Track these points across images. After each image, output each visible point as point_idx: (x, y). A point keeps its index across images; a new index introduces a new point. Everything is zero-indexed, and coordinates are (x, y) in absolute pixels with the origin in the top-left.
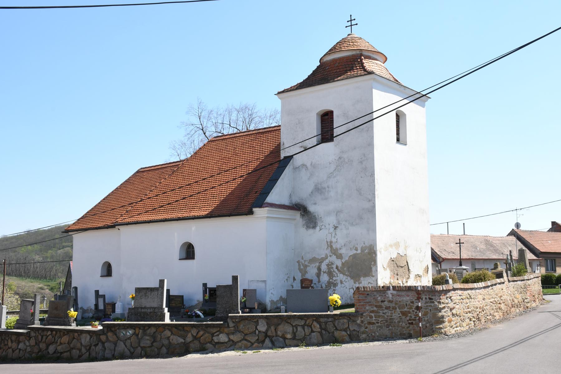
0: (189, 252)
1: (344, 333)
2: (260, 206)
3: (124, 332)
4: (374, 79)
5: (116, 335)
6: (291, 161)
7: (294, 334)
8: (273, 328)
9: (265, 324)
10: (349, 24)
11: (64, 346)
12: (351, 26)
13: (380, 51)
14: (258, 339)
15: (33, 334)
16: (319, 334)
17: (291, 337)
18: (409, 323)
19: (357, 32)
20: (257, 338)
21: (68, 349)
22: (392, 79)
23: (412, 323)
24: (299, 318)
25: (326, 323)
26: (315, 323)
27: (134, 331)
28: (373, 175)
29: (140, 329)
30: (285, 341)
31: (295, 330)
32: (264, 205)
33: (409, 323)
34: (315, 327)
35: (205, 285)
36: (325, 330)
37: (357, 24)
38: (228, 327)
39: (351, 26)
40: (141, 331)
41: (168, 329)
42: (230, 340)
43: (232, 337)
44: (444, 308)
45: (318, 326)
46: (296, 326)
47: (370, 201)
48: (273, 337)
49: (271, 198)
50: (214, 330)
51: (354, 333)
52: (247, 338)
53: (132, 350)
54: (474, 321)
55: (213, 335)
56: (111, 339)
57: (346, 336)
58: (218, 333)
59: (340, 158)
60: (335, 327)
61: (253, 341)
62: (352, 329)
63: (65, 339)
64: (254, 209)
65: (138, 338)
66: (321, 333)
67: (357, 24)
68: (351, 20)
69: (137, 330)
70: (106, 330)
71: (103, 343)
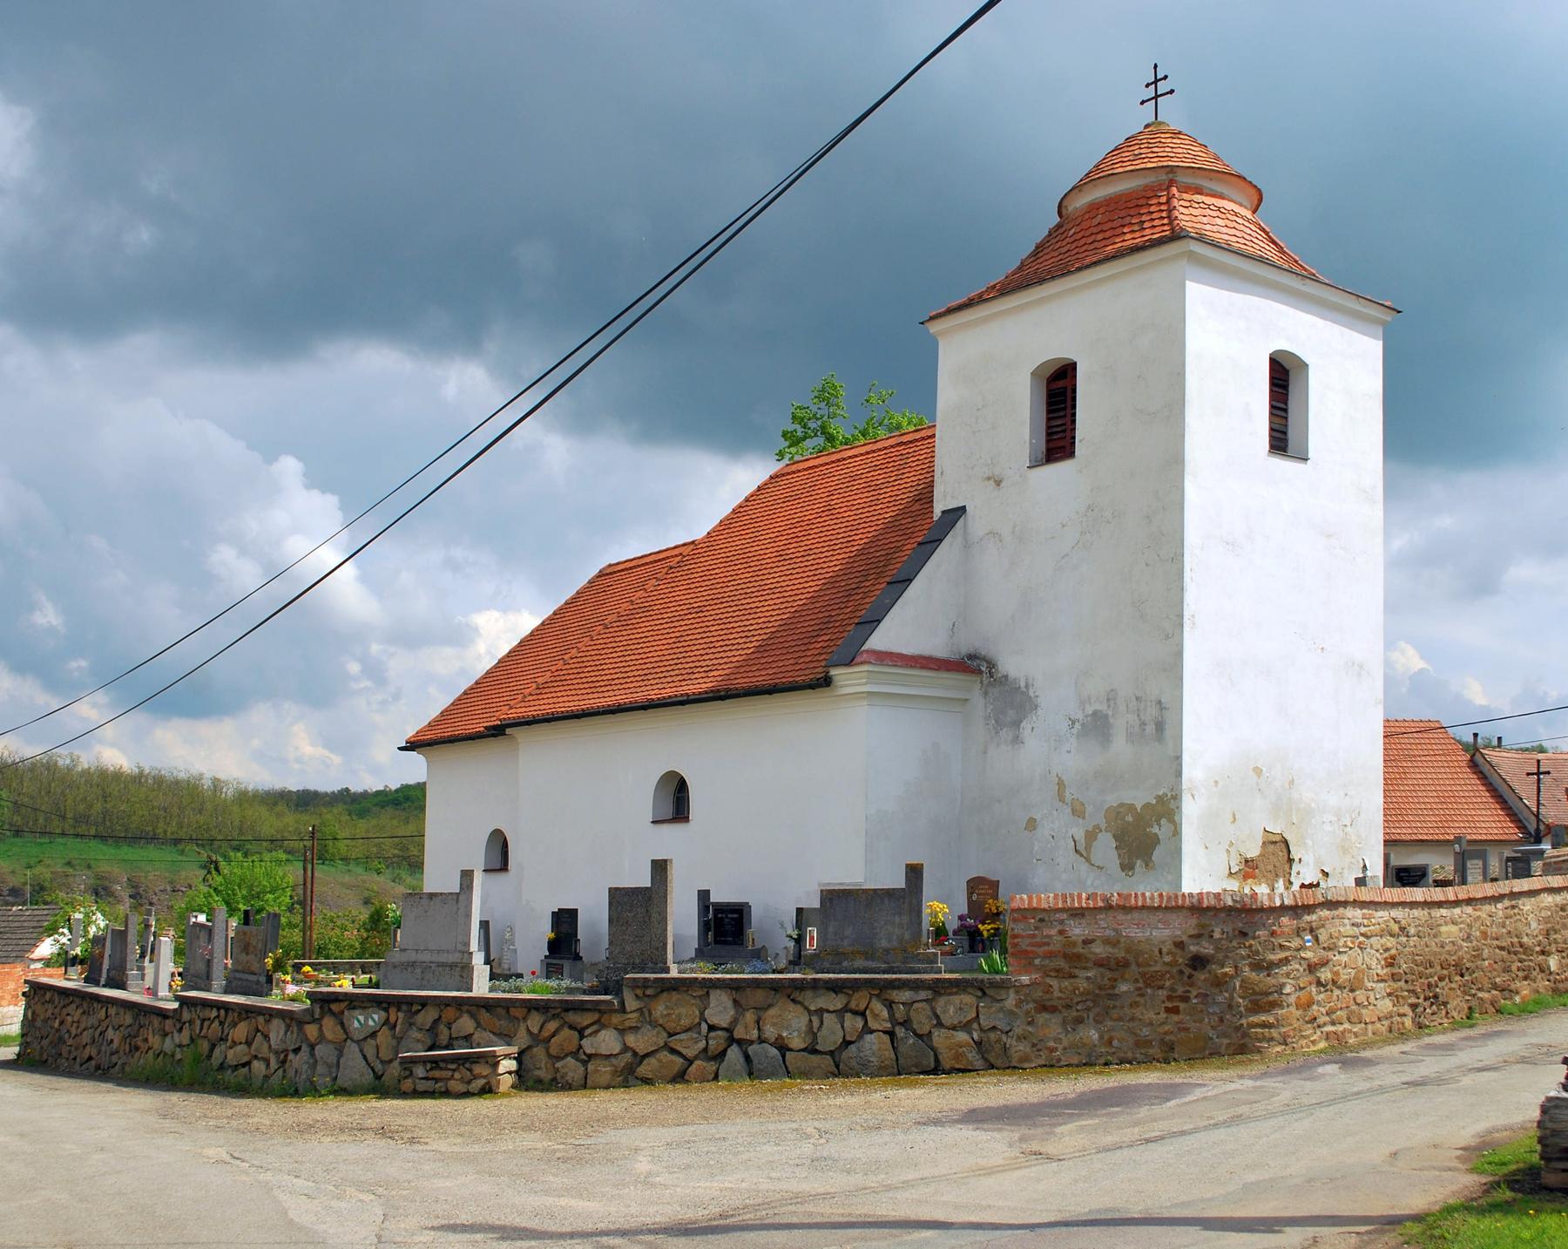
0: (676, 800)
1: (962, 1036)
2: (850, 663)
3: (361, 1018)
4: (1193, 257)
5: (342, 1024)
6: (960, 524)
7: (812, 1034)
8: (750, 1017)
9: (730, 1004)
10: (1151, 92)
11: (239, 1048)
12: (1156, 97)
13: (1237, 168)
14: (705, 1050)
15: (186, 1016)
16: (886, 1038)
17: (803, 1046)
18: (1168, 1010)
19: (1172, 113)
20: (702, 1044)
21: (246, 1059)
22: (1270, 252)
23: (1175, 1010)
24: (828, 989)
25: (908, 1005)
26: (877, 1006)
27: (383, 1014)
28: (1177, 558)
29: (399, 1010)
30: (784, 1057)
31: (816, 1023)
32: (858, 659)
33: (1168, 1010)
34: (876, 1016)
35: (704, 895)
36: (906, 1023)
37: (1172, 92)
38: (623, 1009)
39: (1156, 97)
40: (401, 1015)
41: (468, 1012)
42: (626, 1049)
43: (631, 1040)
44: (1286, 961)
45: (885, 1013)
46: (820, 1012)
47: (1167, 637)
48: (752, 1042)
49: (882, 639)
50: (585, 1019)
51: (992, 1036)
52: (675, 1043)
53: (379, 1067)
54: (1414, 1006)
55: (581, 1034)
56: (329, 1035)
57: (968, 1044)
58: (595, 1027)
59: (1090, 508)
60: (937, 1017)
61: (689, 1053)
62: (985, 1022)
63: (241, 1031)
64: (833, 672)
65: (394, 1036)
66: (891, 1034)
67: (1172, 92)
68: (1156, 81)
69: (393, 1010)
70: (317, 1011)
71: (312, 1047)
